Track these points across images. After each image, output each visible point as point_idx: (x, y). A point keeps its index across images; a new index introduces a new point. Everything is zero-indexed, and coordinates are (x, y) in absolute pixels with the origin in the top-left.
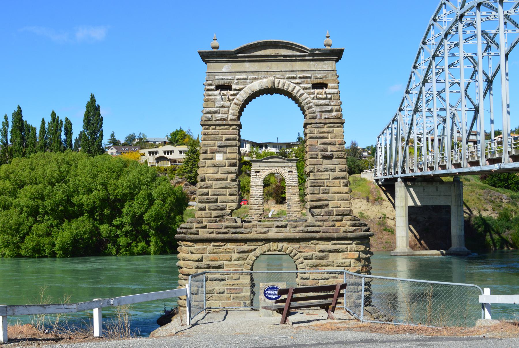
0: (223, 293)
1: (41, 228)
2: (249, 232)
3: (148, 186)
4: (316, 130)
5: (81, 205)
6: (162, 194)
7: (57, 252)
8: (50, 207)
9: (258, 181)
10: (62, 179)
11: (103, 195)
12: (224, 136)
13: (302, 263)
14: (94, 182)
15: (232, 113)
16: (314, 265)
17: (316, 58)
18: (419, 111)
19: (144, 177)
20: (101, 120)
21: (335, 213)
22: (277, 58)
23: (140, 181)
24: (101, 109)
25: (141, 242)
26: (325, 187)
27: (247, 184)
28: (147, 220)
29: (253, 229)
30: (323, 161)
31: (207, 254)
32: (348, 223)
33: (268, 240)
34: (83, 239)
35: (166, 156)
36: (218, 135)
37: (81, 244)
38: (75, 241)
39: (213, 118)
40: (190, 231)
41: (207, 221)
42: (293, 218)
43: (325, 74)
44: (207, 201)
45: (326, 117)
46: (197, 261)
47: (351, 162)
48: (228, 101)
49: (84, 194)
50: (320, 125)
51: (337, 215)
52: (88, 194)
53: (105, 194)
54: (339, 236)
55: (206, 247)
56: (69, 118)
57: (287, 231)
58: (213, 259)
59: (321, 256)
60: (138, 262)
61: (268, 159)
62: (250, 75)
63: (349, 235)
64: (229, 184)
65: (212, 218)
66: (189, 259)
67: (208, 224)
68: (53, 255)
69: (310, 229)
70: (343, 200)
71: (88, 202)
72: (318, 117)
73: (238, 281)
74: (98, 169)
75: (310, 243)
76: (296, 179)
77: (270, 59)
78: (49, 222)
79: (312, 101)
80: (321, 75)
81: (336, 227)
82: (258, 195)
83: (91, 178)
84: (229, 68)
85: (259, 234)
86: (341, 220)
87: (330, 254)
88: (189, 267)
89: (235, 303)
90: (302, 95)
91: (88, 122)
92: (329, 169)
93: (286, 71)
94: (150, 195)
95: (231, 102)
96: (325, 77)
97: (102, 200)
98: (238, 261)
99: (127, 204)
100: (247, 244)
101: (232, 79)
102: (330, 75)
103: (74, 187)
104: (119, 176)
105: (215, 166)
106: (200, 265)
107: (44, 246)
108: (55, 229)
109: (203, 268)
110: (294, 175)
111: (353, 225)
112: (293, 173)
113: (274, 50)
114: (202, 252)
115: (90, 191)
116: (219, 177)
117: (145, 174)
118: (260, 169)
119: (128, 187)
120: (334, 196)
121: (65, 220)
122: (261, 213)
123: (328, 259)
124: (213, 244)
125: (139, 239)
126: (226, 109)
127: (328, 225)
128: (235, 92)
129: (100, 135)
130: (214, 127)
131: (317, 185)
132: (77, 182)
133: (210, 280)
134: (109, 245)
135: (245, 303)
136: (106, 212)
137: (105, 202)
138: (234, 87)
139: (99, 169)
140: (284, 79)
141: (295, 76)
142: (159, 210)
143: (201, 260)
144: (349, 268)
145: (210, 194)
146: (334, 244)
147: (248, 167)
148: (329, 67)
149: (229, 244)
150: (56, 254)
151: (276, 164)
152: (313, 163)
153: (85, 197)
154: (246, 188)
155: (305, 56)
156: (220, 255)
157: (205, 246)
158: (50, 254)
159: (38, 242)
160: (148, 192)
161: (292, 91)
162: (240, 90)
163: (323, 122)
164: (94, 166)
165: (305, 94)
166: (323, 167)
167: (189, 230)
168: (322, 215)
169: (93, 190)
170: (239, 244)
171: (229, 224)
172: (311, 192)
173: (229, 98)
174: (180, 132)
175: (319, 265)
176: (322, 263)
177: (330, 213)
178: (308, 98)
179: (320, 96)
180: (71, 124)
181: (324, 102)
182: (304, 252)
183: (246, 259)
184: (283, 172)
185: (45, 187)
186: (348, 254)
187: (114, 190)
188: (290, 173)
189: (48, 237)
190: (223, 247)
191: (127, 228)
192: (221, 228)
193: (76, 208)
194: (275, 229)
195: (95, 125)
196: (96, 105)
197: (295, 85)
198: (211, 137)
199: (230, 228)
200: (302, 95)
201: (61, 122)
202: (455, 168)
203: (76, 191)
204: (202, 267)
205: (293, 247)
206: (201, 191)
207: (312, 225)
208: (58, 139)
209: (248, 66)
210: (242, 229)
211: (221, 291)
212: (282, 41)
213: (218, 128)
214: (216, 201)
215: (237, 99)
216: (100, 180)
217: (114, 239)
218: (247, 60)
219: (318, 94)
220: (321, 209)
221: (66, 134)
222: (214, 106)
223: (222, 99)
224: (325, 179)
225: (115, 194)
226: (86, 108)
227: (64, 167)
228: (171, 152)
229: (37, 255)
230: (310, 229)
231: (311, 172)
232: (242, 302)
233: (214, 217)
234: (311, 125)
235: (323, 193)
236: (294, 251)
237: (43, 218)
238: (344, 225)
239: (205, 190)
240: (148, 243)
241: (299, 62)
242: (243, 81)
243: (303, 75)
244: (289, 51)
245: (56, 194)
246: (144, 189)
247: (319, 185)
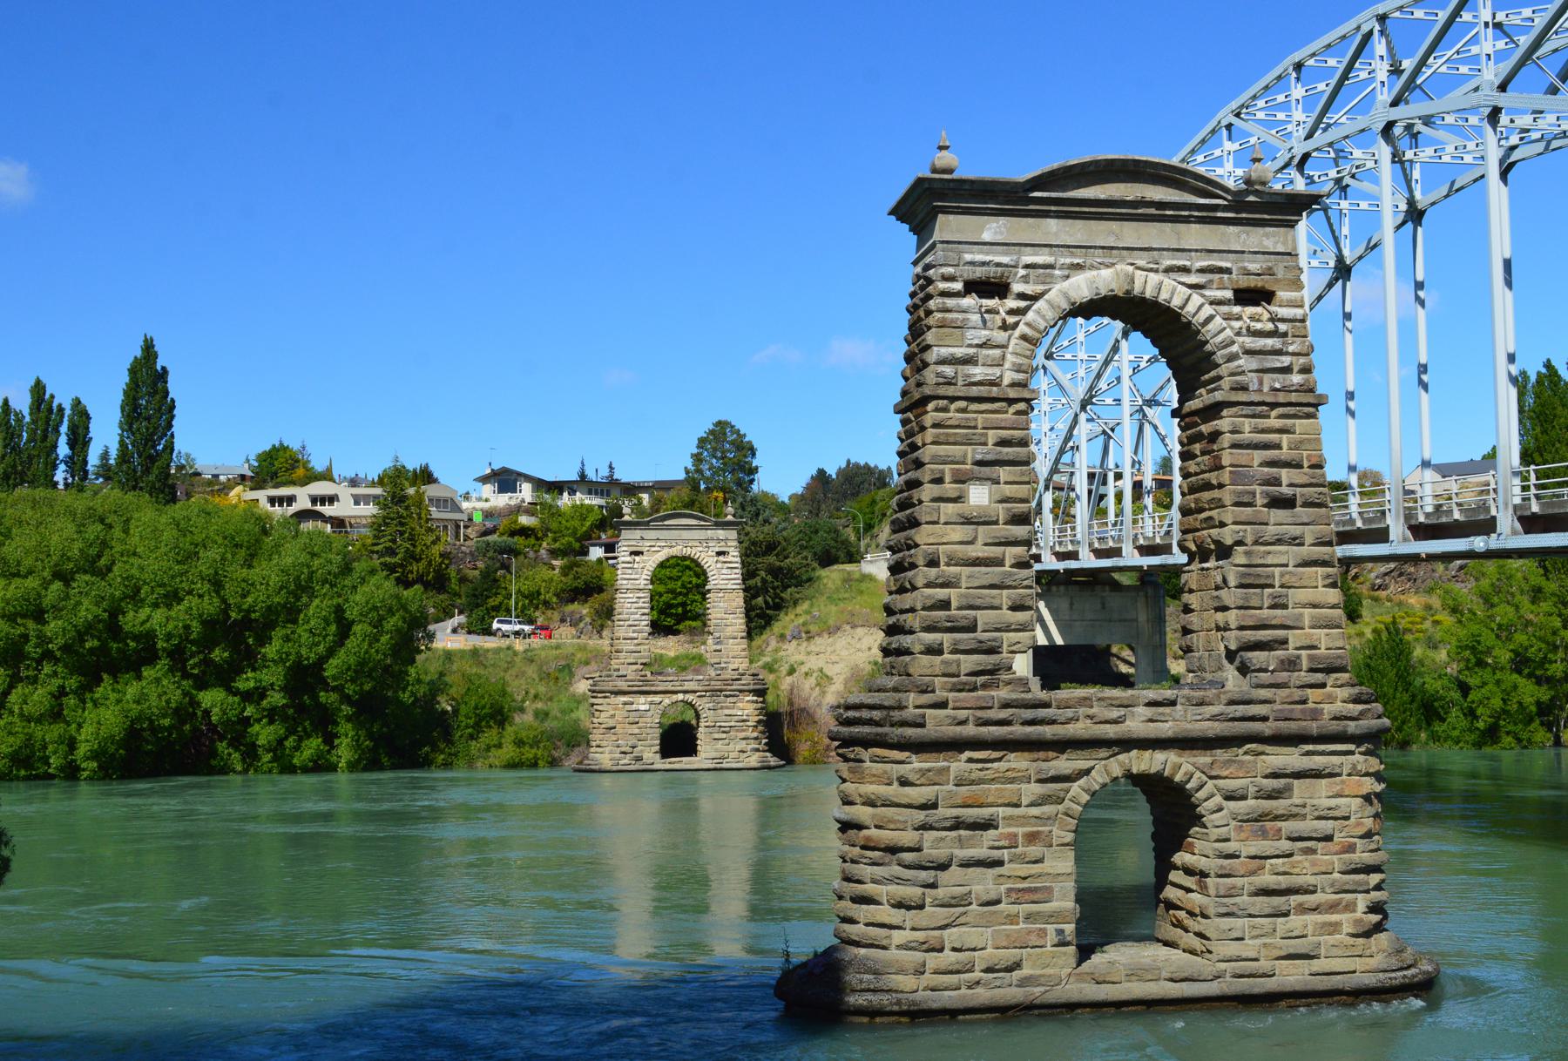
0: (998, 902)
1: (38, 697)
2: (1071, 719)
3: (332, 586)
4: (1247, 424)
5: (150, 636)
6: (375, 608)
7: (84, 765)
8: (61, 641)
9: (637, 576)
10: (94, 565)
11: (212, 610)
12: (991, 432)
13: (1220, 809)
14: (187, 572)
15: (1014, 364)
16: (1255, 815)
17: (1244, 215)
18: (1093, 404)
19: (322, 560)
20: (168, 409)
21: (1305, 664)
22: (1140, 211)
23: (313, 572)
24: (170, 378)
25: (309, 736)
26: (1277, 589)
27: (544, 584)
28: (334, 678)
29: (1082, 711)
30: (1269, 513)
31: (951, 787)
32: (1345, 693)
33: (1127, 744)
34: (154, 729)
35: (318, 508)
36: (975, 427)
37: (148, 742)
38: (133, 734)
39: (960, 379)
40: (896, 715)
41: (949, 686)
42: (729, 675)
44: (949, 624)
45: (1277, 386)
46: (923, 807)
47: (828, 533)
48: (1000, 328)
49: (156, 605)
50: (1260, 408)
51: (1311, 670)
52: (169, 607)
53: (219, 607)
54: (1324, 731)
55: (945, 764)
56: (83, 401)
57: (1177, 717)
58: (970, 802)
59: (1274, 790)
60: (304, 795)
61: (665, 520)
62: (1062, 256)
63: (1352, 727)
64: (1011, 574)
65: (964, 679)
66: (895, 800)
67: (951, 695)
68: (71, 772)
69: (1241, 710)
70: (1325, 627)
71: (170, 627)
72: (1254, 386)
73: (1040, 865)
74: (195, 538)
75: (1241, 751)
76: (737, 574)
77: (1118, 211)
78: (57, 682)
79: (1236, 338)
80: (1258, 266)
81: (1310, 705)
82: (636, 613)
83: (179, 563)
84: (1002, 233)
86: (1323, 686)
87: (1296, 782)
88: (892, 826)
89: (1029, 932)
90: (1210, 319)
91: (132, 412)
92: (1287, 536)
93: (1164, 249)
94: (339, 610)
95: (1010, 332)
96: (1270, 272)
97: (209, 624)
98: (1040, 805)
99: (278, 634)
100: (1065, 756)
101: (1012, 263)
102: (1281, 265)
103: (126, 586)
104: (252, 556)
105: (968, 521)
106: (930, 820)
107: (45, 747)
108: (71, 701)
109: (938, 830)
110: (730, 562)
111: (1356, 700)
112: (730, 559)
113: (1129, 185)
114: (937, 779)
115: (173, 598)
116: (980, 555)
117: (322, 554)
118: (644, 547)
119: (281, 588)
120: (1301, 615)
121: (105, 676)
122: (644, 661)
123: (1290, 797)
124: (968, 754)
125: (305, 729)
126: (997, 352)
127: (1289, 700)
128: (1023, 304)
129: (165, 448)
130: (962, 404)
131: (1257, 582)
132: (134, 572)
133: (961, 866)
134: (222, 747)
135: (1060, 932)
136: (219, 654)
137: (218, 628)
138: (1017, 287)
139: (199, 538)
140: (1156, 271)
141: (1188, 263)
142: (366, 652)
143: (934, 806)
144: (1347, 823)
145: (954, 604)
146: (1308, 753)
147: (532, 541)
148: (1279, 245)
149: (1013, 755)
150: (78, 769)
151: (686, 534)
152: (1243, 518)
153: (159, 615)
154: (542, 597)
155: (1215, 208)
156: (989, 789)
157: (945, 760)
158: (61, 769)
159: (30, 737)
160: (335, 602)
161: (1182, 308)
162: (1034, 298)
163: (1269, 399)
164: (182, 529)
165: (1218, 320)
166: (1271, 530)
167: (892, 713)
168: (1271, 668)
169: (182, 594)
170: (1042, 754)
171: (1014, 696)
172: (1240, 603)
173: (1004, 321)
174: (281, 453)
175: (1267, 815)
176: (1277, 808)
177: (1291, 665)
178: (1225, 329)
179: (1258, 326)
180: (88, 418)
181: (1270, 342)
183: (1064, 800)
184: (703, 555)
185: (46, 584)
186: (1343, 782)
187: (244, 596)
189: (55, 722)
190: (996, 765)
191: (276, 698)
192: (990, 708)
193: (132, 644)
194: (1142, 711)
195: (153, 421)
196: (159, 368)
197: (1190, 291)
198: (956, 434)
199: (1016, 707)
200: (1210, 319)
201: (61, 409)
202: (1141, 555)
203: (134, 596)
204: (937, 825)
205: (1193, 765)
206: (929, 597)
207: (1246, 697)
208: (48, 455)
209: (1053, 228)
210: (1050, 710)
211: (993, 896)
212: (1157, 160)
213: (974, 406)
214: (972, 628)
215: (1028, 324)
216: (203, 567)
217: (238, 727)
218: (1055, 212)
219: (1252, 318)
220: (1266, 653)
221: (72, 444)
222: (959, 343)
223: (984, 321)
224: (1276, 566)
225: (245, 607)
226: (127, 373)
227: (95, 529)
228: (332, 499)
229: (23, 772)
230: (1241, 710)
231: (1240, 543)
232: (1051, 928)
233: (966, 675)
234: (1234, 410)
235: (1272, 607)
236: (1198, 774)
237: (36, 669)
238: (1331, 699)
239: (941, 593)
240: (330, 739)
241: (1197, 226)
242: (1041, 271)
243: (1210, 263)
244: (1171, 191)
245: (79, 603)
246: (325, 595)
247: (1262, 581)
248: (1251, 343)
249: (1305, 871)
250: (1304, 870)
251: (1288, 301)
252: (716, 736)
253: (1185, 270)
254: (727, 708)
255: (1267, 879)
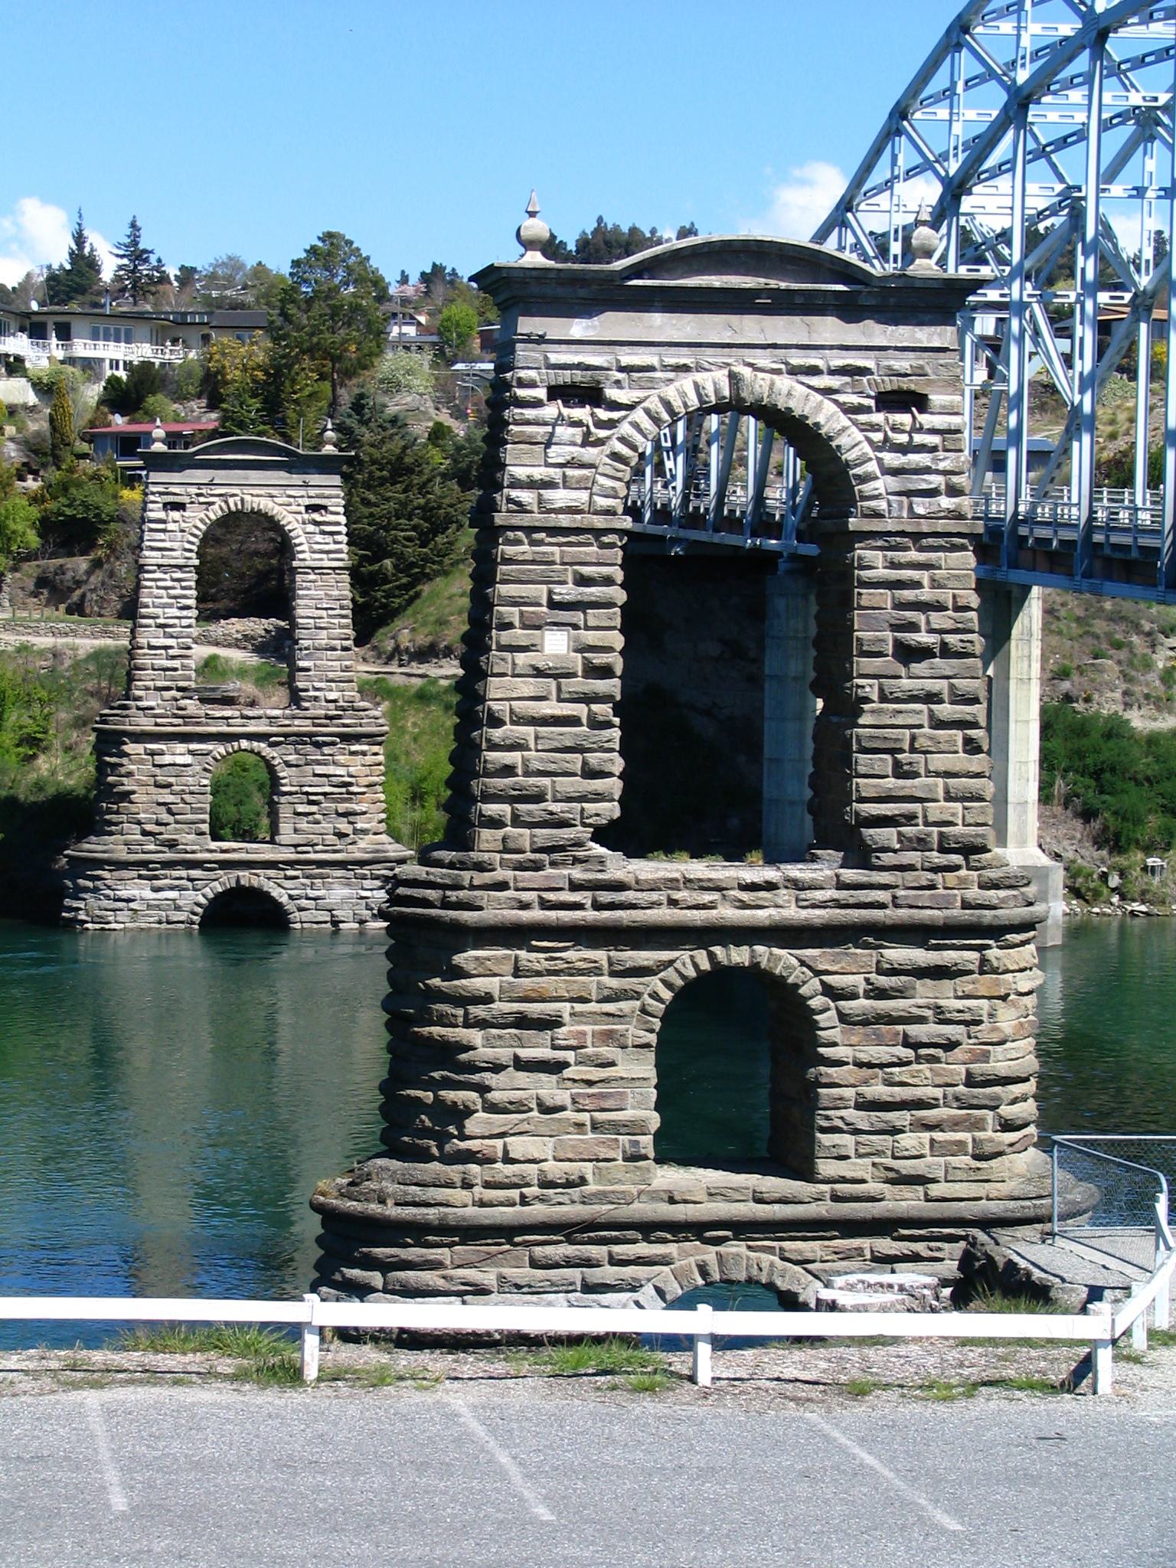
36: (553, 563)
40: (453, 895)
43: (921, 362)
82: (171, 606)
85: (684, 911)
105: (539, 673)
118: (181, 493)
148: (935, 337)
182: (836, 973)
188: (316, 516)
198: (530, 571)
248: (892, 459)
249: (925, 1082)
250: (922, 1081)
251: (944, 407)
252: (301, 809)
253: (814, 371)
254: (319, 763)
255: (878, 1090)
